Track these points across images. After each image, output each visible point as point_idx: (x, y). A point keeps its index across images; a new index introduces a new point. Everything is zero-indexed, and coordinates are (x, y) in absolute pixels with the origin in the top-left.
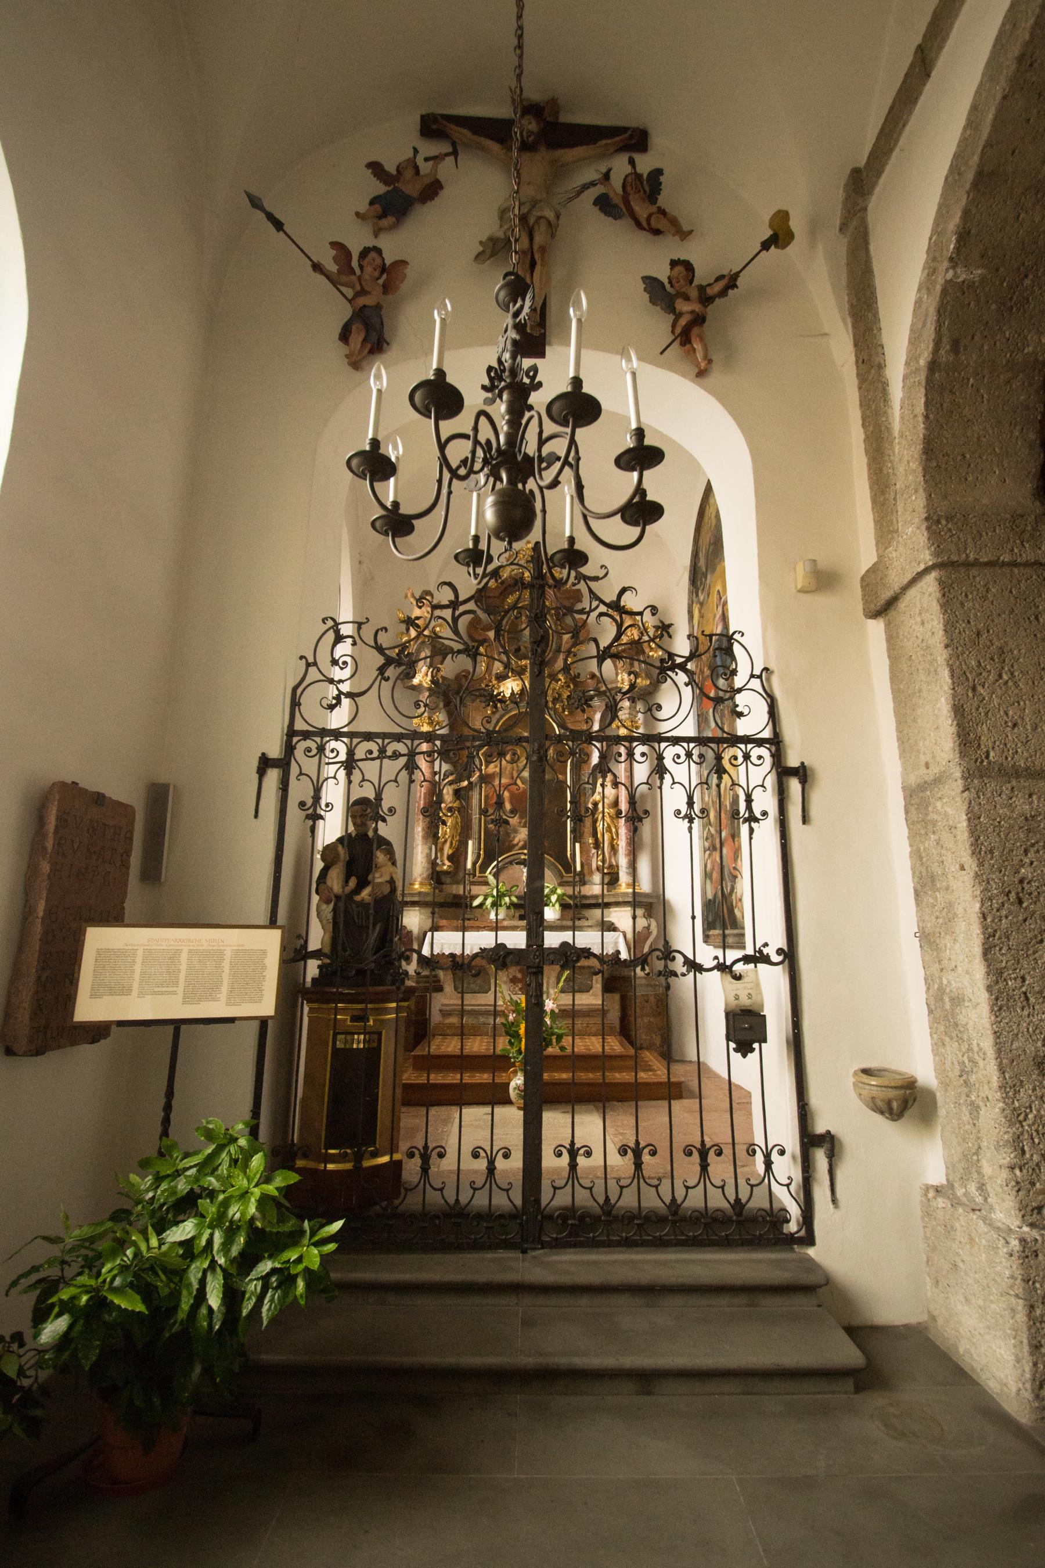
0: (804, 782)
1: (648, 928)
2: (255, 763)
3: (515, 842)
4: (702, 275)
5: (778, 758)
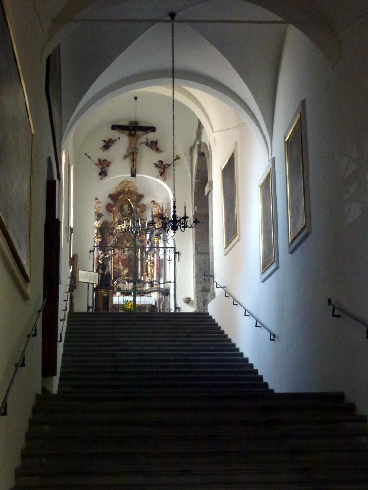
0: (179, 254)
1: (162, 298)
2: (89, 251)
3: (123, 274)
4: (164, 164)
5: (175, 250)
